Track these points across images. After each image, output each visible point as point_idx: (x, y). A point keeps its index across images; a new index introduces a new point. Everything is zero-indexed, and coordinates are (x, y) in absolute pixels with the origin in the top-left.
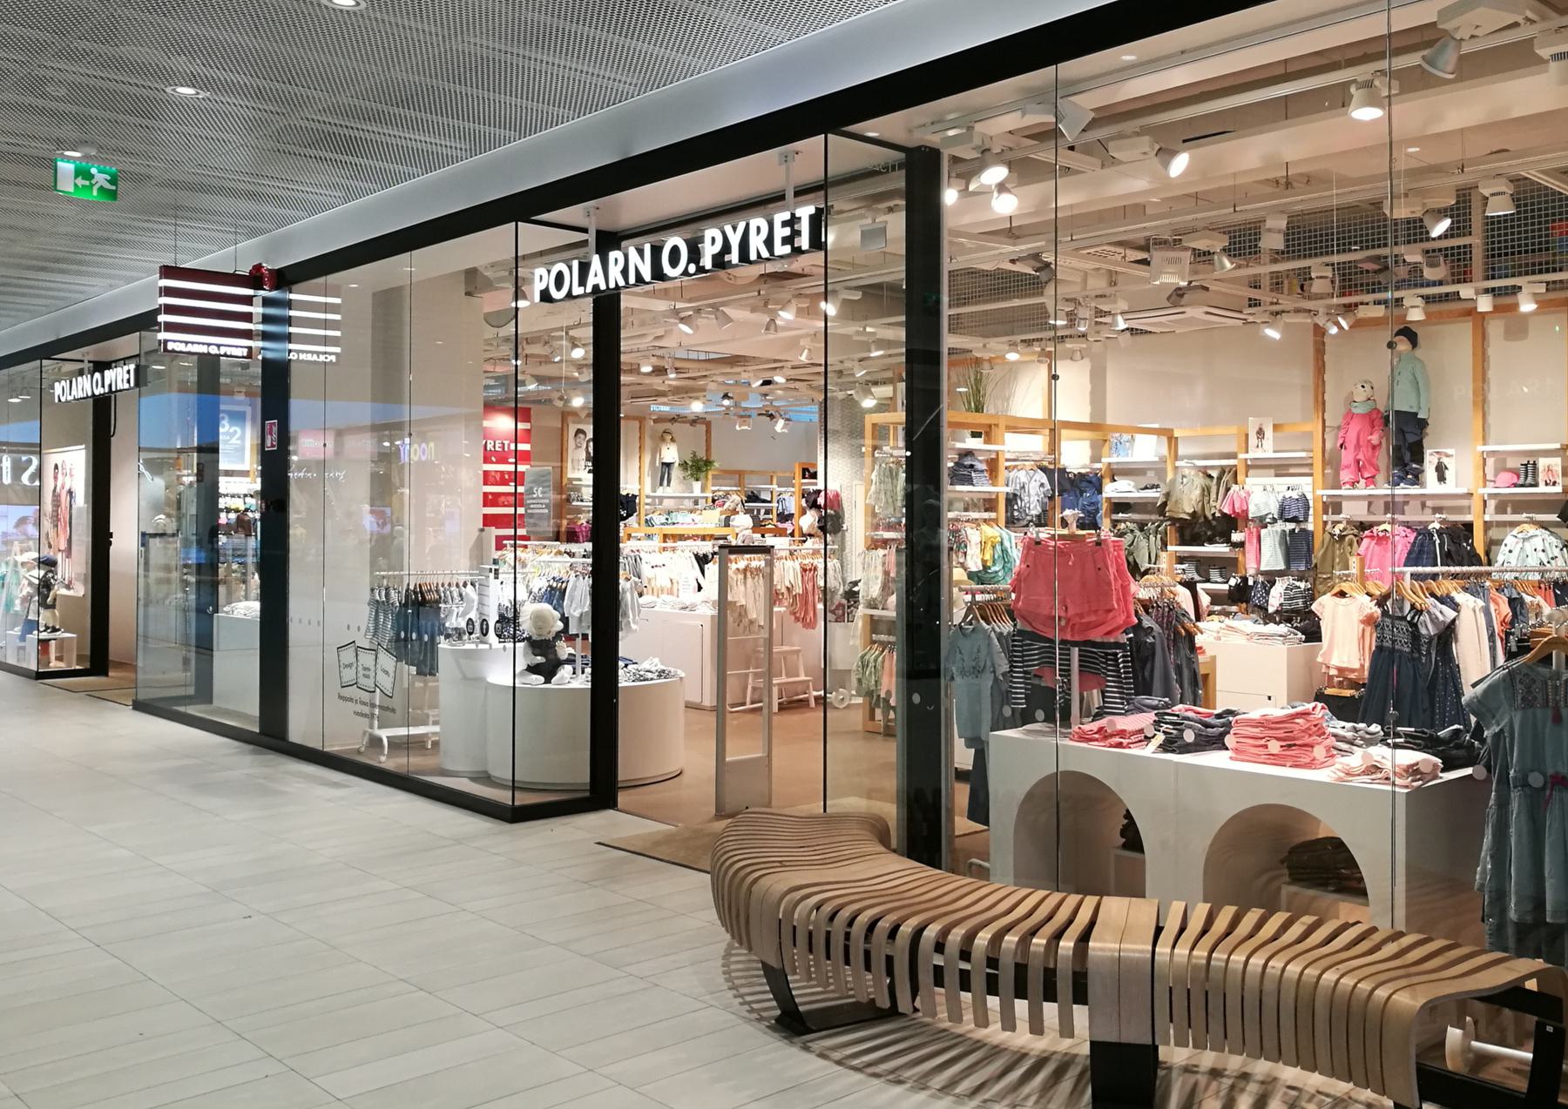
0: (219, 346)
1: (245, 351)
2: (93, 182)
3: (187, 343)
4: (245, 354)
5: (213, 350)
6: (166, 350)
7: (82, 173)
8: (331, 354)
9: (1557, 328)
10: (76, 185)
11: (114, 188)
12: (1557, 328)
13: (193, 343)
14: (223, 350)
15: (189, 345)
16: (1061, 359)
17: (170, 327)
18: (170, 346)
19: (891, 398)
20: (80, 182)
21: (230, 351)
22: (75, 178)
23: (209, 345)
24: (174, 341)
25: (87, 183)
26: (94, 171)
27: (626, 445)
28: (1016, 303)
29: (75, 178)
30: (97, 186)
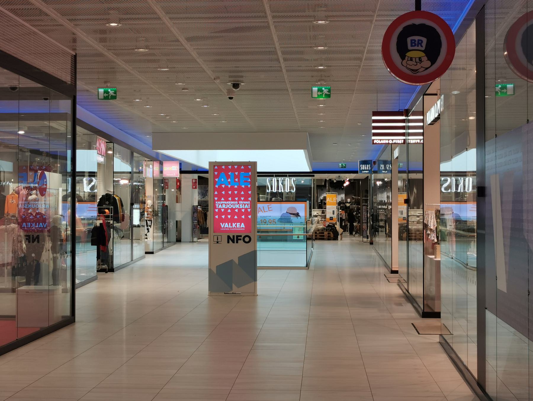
0: (392, 140)
1: (403, 141)
2: (323, 92)
3: (381, 140)
4: (402, 142)
5: (391, 142)
6: (373, 143)
7: (320, 90)
8: (418, 139)
9: (506, 53)
10: (318, 95)
11: (329, 93)
12: (506, 53)
13: (383, 140)
14: (394, 141)
15: (384, 140)
16: (421, 179)
17: (375, 134)
18: (375, 142)
19: (8, 266)
20: (319, 93)
21: (396, 142)
22: (318, 92)
23: (389, 140)
24: (376, 140)
25: (321, 93)
26: (323, 89)
27: (115, 251)
28: (418, 102)
29: (318, 92)
30: (324, 94)
